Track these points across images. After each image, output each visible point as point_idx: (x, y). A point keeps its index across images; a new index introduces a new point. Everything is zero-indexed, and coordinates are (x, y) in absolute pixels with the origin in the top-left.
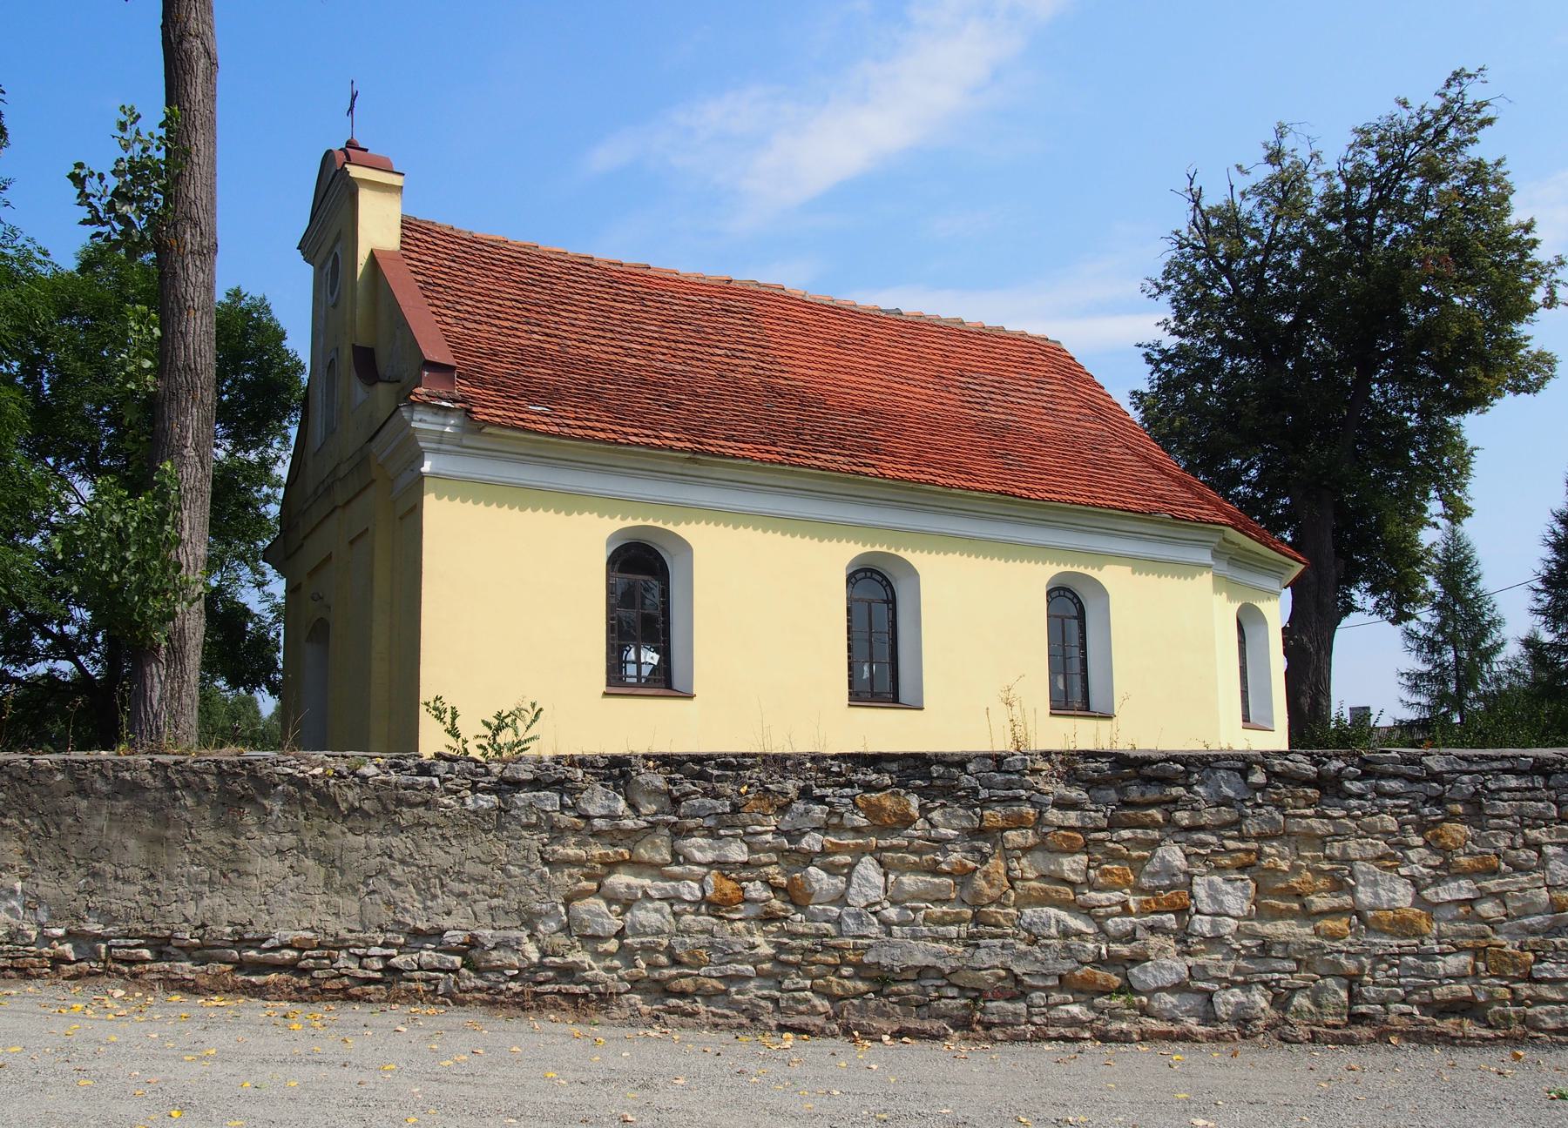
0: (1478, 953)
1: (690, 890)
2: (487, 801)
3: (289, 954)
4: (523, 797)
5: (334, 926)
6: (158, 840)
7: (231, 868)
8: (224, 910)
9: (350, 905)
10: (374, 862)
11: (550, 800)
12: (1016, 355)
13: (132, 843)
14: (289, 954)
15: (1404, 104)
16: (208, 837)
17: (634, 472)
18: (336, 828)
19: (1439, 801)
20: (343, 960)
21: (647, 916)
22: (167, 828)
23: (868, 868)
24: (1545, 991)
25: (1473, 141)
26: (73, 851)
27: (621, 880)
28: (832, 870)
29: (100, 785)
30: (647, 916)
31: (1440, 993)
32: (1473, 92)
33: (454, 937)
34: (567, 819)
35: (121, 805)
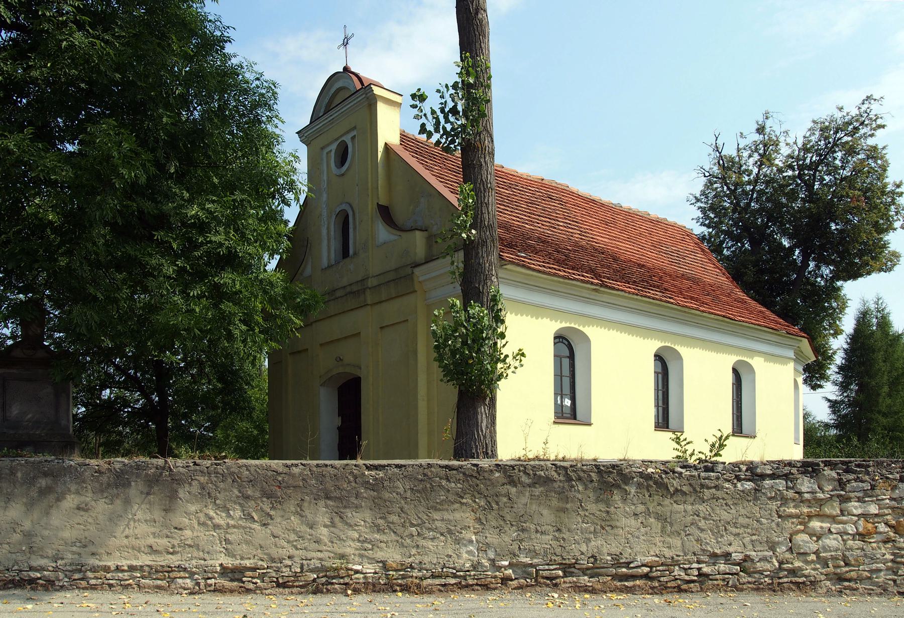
1: (851, 529)
2: (749, 485)
3: (646, 570)
4: (768, 483)
5: (668, 553)
6: (564, 510)
7: (607, 524)
8: (605, 547)
9: (677, 542)
10: (689, 519)
11: (781, 484)
12: (679, 236)
13: (545, 512)
14: (646, 570)
15: (841, 109)
16: (592, 507)
17: (734, 334)
18: (667, 502)
20: (677, 571)
21: (832, 542)
22: (567, 503)
25: (872, 135)
26: (508, 517)
29: (525, 479)
30: (832, 542)
32: (875, 108)
33: (737, 557)
35: (538, 490)
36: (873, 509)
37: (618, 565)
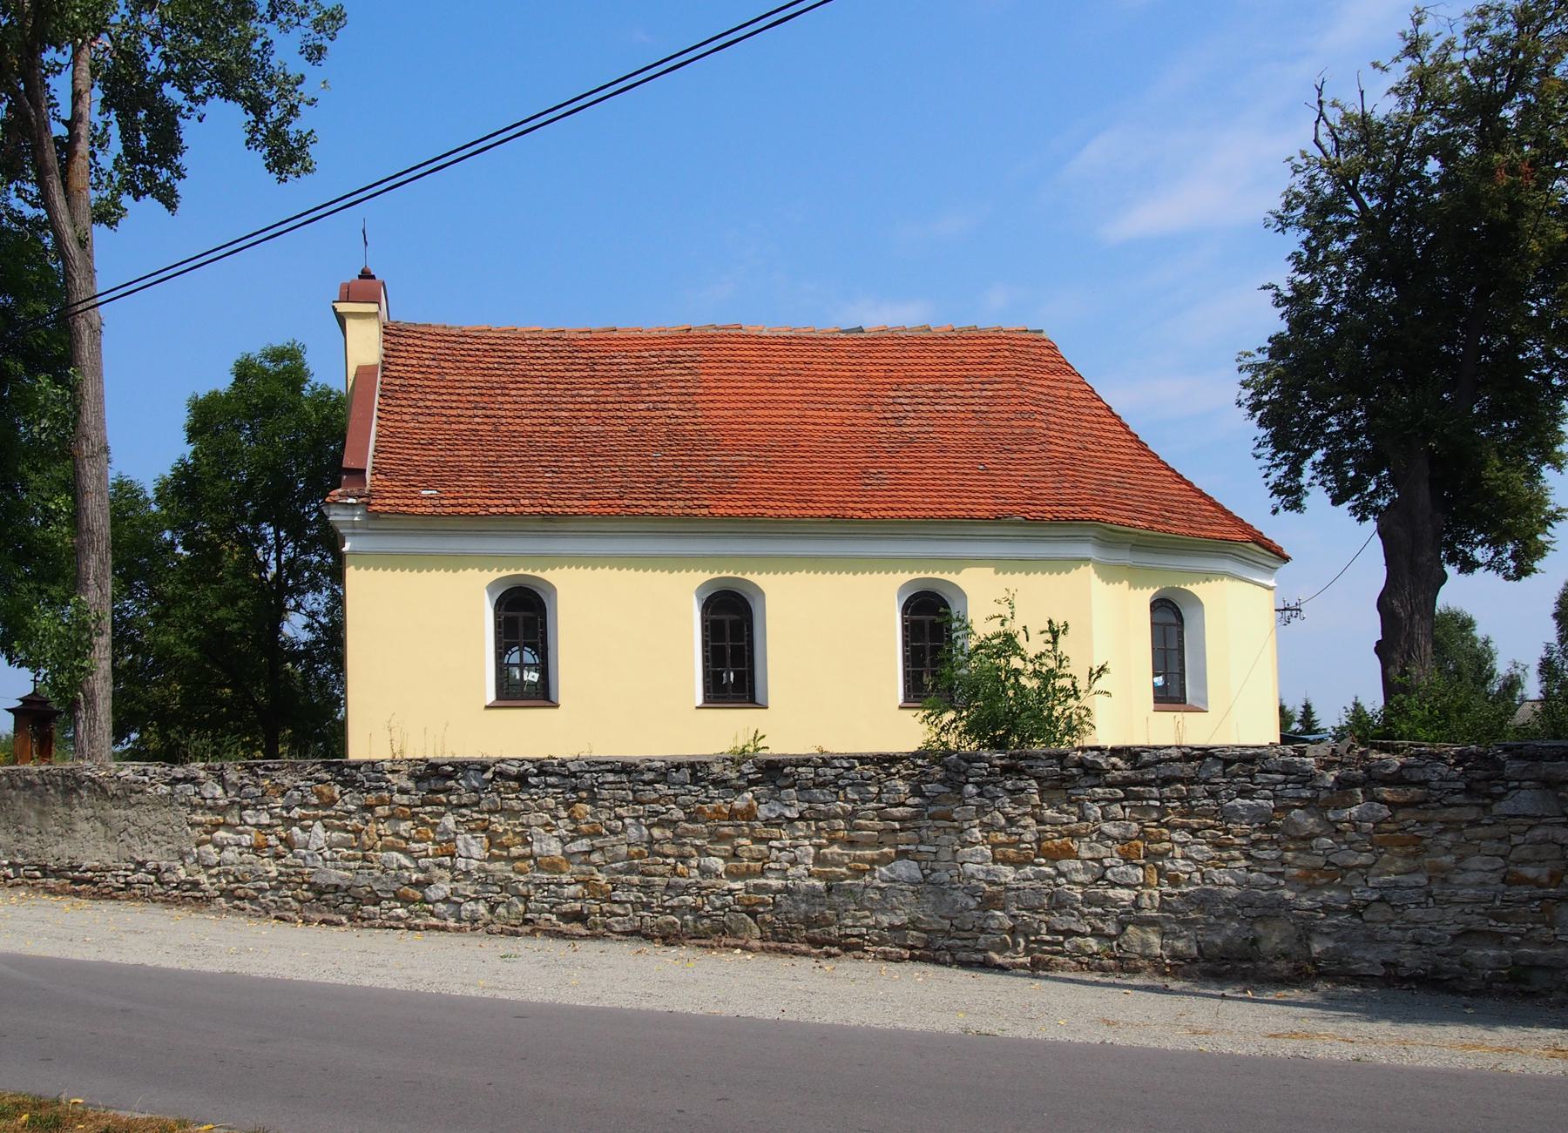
0: (585, 883)
1: (246, 840)
3: (90, 874)
7: (69, 828)
19: (575, 789)
23: (318, 828)
24: (617, 909)
27: (221, 834)
28: (304, 829)
30: (229, 855)
31: (565, 908)
33: (150, 866)
34: (196, 800)
36: (265, 819)
37: (73, 868)
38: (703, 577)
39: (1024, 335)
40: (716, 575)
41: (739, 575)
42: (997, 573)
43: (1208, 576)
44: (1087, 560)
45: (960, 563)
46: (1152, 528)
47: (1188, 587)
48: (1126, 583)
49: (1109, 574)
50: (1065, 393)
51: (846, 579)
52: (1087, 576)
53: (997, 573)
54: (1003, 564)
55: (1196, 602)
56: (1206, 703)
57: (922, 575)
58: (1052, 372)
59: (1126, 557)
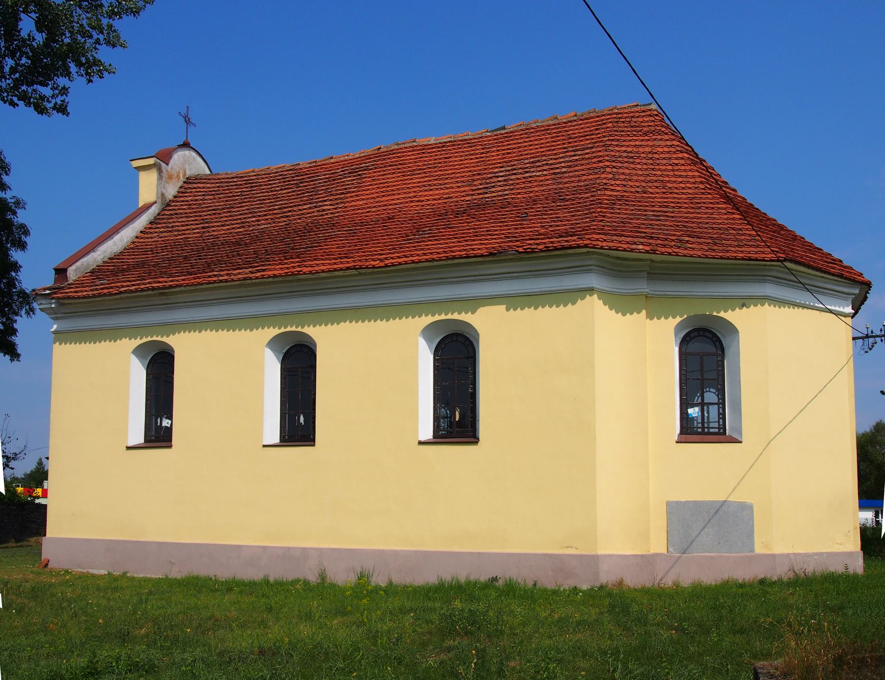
38: (273, 332)
39: (636, 109)
40: (283, 330)
41: (299, 329)
42: (508, 310)
43: (744, 302)
44: (590, 290)
45: (474, 303)
46: (654, 252)
47: (722, 314)
48: (16, 255)
49: (621, 304)
50: (647, 149)
51: (380, 325)
52: (594, 308)
53: (508, 310)
54: (514, 301)
55: (732, 330)
56: (741, 433)
57: (443, 317)
58: (645, 134)
59: (643, 287)
